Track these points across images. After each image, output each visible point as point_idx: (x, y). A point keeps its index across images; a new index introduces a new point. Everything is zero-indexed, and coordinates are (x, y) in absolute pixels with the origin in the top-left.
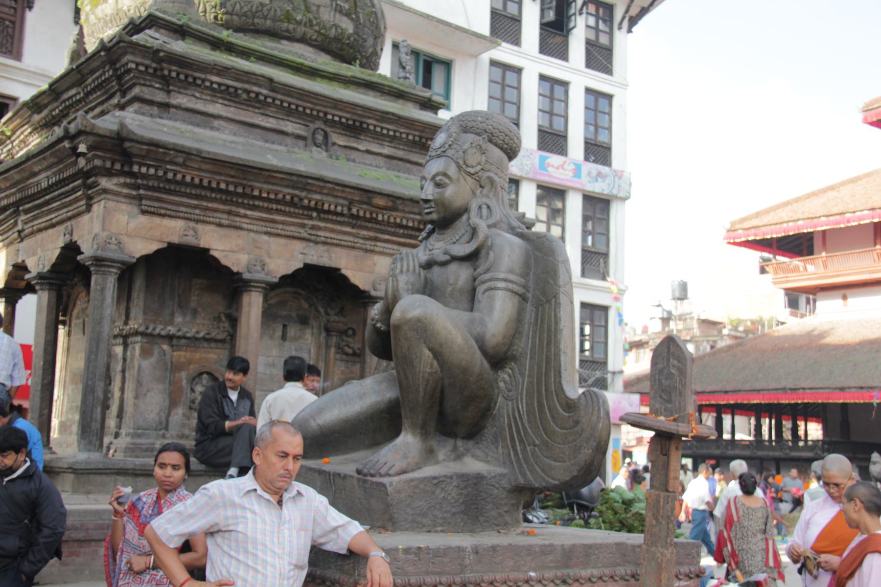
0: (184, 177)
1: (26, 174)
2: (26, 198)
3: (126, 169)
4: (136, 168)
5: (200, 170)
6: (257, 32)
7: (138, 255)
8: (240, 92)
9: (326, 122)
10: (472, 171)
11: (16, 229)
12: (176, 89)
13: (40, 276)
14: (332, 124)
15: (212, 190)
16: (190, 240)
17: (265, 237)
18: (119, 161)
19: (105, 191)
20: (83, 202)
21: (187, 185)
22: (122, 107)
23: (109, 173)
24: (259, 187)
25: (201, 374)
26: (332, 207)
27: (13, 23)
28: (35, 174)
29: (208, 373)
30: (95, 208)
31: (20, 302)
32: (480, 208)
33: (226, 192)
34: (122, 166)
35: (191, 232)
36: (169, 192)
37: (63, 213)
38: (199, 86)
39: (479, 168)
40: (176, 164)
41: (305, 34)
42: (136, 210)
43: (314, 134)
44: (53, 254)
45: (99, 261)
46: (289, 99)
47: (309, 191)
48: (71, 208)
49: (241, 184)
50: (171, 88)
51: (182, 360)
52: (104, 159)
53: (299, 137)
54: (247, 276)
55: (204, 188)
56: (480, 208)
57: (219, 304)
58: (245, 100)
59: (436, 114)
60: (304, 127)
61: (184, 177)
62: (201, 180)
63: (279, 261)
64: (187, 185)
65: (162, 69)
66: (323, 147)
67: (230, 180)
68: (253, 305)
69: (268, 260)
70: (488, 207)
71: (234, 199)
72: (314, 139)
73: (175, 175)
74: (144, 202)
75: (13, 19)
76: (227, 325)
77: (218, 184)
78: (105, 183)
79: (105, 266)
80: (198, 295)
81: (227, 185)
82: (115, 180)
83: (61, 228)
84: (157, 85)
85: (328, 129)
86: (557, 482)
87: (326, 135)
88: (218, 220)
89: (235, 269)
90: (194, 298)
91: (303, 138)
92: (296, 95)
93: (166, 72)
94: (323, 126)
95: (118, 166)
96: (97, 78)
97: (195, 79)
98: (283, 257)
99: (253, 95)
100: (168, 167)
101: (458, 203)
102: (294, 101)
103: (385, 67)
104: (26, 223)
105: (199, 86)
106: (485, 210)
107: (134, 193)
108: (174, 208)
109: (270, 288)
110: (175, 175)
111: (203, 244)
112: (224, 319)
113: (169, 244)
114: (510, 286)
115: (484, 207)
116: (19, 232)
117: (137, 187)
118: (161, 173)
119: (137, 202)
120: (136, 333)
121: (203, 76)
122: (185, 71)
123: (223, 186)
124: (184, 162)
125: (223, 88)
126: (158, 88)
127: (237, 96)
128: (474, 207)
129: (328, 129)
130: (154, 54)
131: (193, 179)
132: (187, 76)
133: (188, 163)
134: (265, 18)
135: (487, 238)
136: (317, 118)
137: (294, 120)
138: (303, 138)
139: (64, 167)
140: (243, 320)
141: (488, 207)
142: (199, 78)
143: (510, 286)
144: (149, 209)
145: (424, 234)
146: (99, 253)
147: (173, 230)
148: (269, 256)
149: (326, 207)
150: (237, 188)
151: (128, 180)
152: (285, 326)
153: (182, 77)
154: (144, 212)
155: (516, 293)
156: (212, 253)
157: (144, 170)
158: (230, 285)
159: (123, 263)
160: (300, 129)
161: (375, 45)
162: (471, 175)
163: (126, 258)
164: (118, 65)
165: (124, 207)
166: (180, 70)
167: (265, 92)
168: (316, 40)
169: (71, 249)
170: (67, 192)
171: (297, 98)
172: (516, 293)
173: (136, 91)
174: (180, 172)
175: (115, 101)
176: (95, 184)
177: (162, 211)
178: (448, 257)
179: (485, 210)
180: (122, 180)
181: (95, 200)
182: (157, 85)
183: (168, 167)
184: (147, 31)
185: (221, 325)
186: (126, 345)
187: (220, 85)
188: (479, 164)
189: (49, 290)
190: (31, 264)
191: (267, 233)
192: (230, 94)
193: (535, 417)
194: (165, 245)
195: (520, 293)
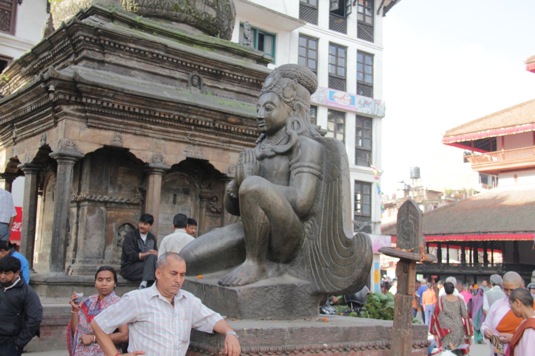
0: (113, 105)
1: (18, 104)
2: (18, 118)
3: (78, 100)
4: (84, 100)
5: (123, 101)
6: (158, 17)
7: (85, 153)
8: (147, 53)
9: (200, 71)
10: (288, 100)
11: (12, 137)
13: (27, 166)
14: (203, 72)
15: (131, 113)
17: (163, 142)
18: (74, 96)
19: (66, 114)
21: (115, 110)
27: (10, 12)
28: (23, 104)
29: (128, 224)
30: (60, 124)
31: (15, 181)
32: (293, 123)
33: (139, 114)
34: (76, 98)
35: (118, 139)
37: (40, 128)
38: (123, 50)
39: (292, 99)
40: (108, 97)
41: (186, 18)
42: (84, 125)
43: (192, 79)
44: (34, 152)
45: (62, 156)
46: (177, 58)
47: (189, 113)
49: (148, 109)
50: (105, 51)
51: (113, 216)
52: (65, 95)
54: (152, 165)
55: (126, 112)
56: (293, 123)
57: (135, 182)
58: (150, 58)
59: (266, 66)
60: (186, 75)
62: (124, 107)
64: (115, 110)
66: (198, 87)
67: (141, 107)
68: (156, 183)
70: (298, 122)
71: (144, 119)
72: (192, 82)
73: (108, 104)
75: (10, 10)
76: (140, 194)
77: (134, 109)
78: (65, 109)
79: (65, 159)
81: (140, 110)
82: (72, 107)
83: (39, 137)
84: (97, 50)
85: (201, 76)
86: (340, 289)
88: (134, 131)
89: (145, 161)
91: (186, 81)
92: (181, 55)
93: (102, 42)
94: (198, 74)
95: (73, 99)
96: (61, 46)
97: (120, 45)
99: (155, 55)
100: (104, 99)
101: (280, 120)
102: (180, 59)
103: (236, 38)
104: (18, 134)
105: (123, 50)
106: (296, 125)
107: (83, 115)
108: (108, 124)
109: (166, 172)
110: (108, 104)
112: (138, 191)
114: (311, 170)
115: (296, 123)
116: (14, 139)
117: (85, 111)
118: (99, 103)
121: (125, 44)
122: (114, 41)
123: (137, 110)
124: (113, 96)
125: (137, 51)
128: (289, 122)
131: (119, 106)
132: (115, 44)
133: (116, 97)
136: (194, 69)
137: (180, 70)
138: (186, 81)
139: (41, 99)
141: (298, 122)
142: (123, 45)
143: (311, 170)
144: (92, 125)
145: (259, 139)
146: (62, 151)
147: (107, 137)
148: (165, 153)
149: (200, 123)
150: (146, 112)
152: (175, 195)
153: (112, 44)
154: (89, 127)
155: (315, 175)
156: (131, 151)
157: (89, 101)
159: (77, 157)
160: (184, 76)
161: (229, 25)
162: (287, 103)
163: (78, 154)
164: (73, 38)
165: (77, 123)
166: (111, 40)
168: (193, 22)
169: (45, 149)
170: (43, 114)
171: (182, 57)
172: (315, 175)
173: (84, 53)
174: (111, 102)
175: (71, 59)
176: (60, 110)
178: (273, 153)
179: (296, 125)
180: (76, 107)
183: (104, 99)
184: (91, 17)
185: (137, 195)
186: (79, 207)
188: (292, 96)
189: (32, 174)
190: (21, 158)
191: (164, 139)
194: (102, 146)
195: (317, 174)
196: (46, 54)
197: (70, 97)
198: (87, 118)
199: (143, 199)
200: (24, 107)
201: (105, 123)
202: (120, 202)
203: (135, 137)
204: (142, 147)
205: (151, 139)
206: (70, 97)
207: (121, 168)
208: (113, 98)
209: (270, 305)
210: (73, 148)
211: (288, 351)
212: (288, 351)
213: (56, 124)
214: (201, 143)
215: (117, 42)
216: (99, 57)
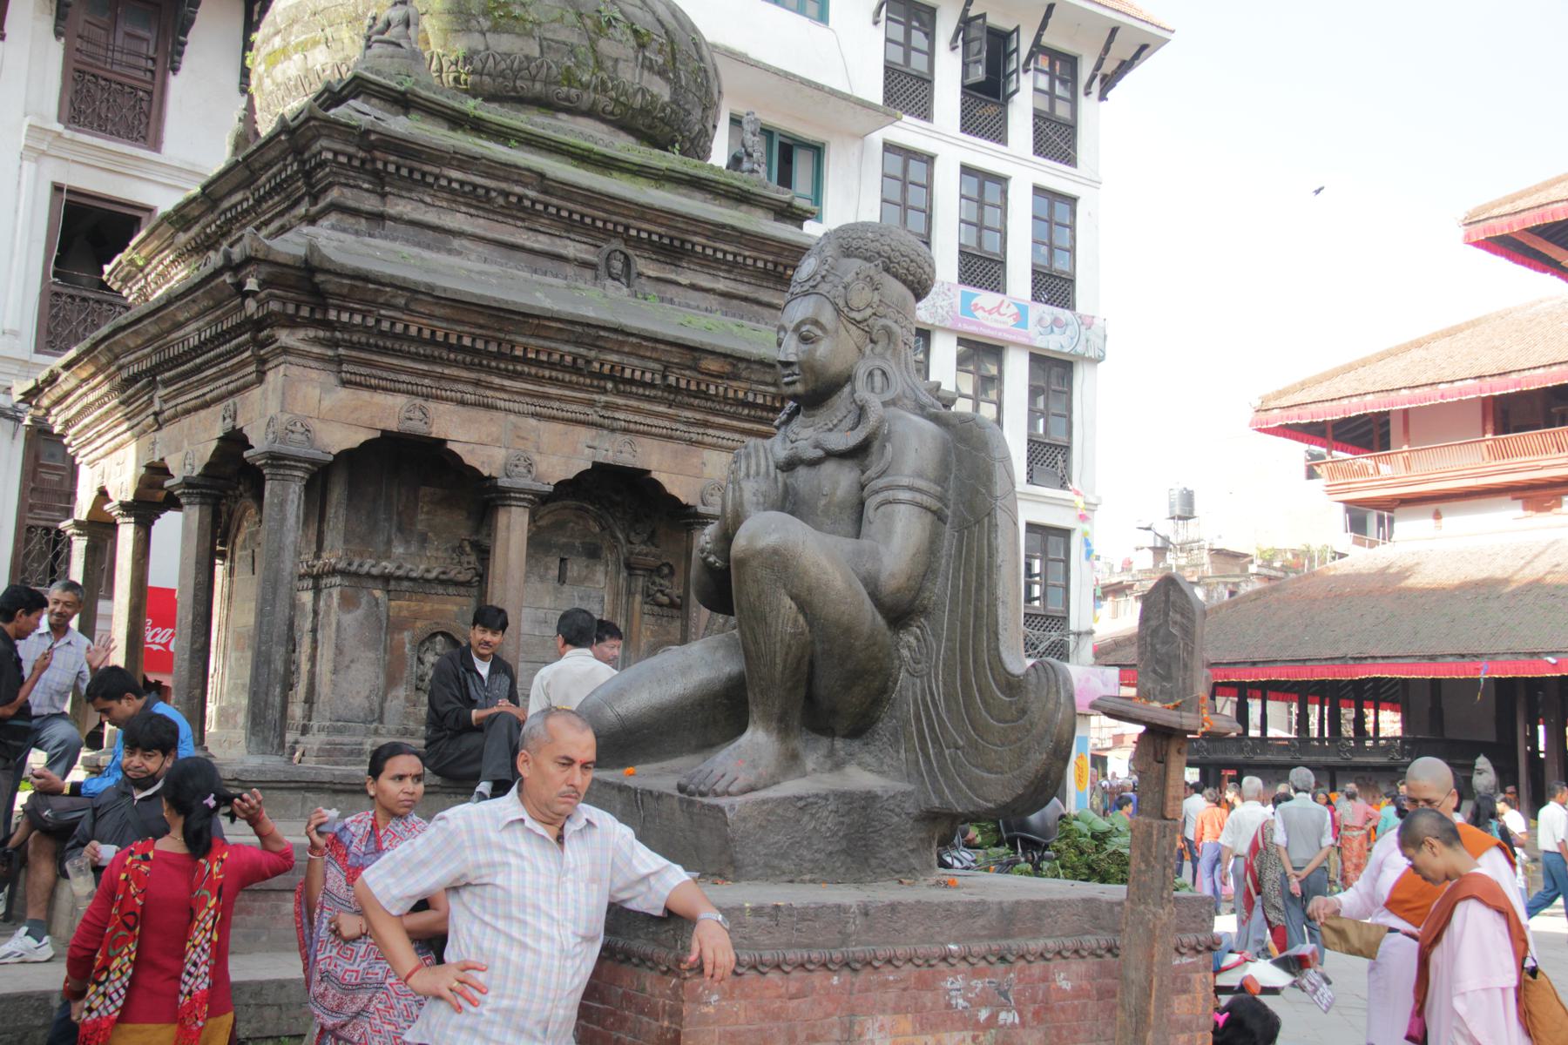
0: (406, 327)
1: (166, 325)
3: (318, 316)
5: (431, 316)
7: (335, 451)
8: (493, 194)
9: (627, 240)
10: (858, 316)
11: (151, 411)
12: (395, 191)
13: (188, 483)
14: (637, 243)
15: (451, 348)
16: (417, 427)
17: (533, 422)
18: (307, 303)
19: (286, 350)
20: (252, 368)
22: (312, 220)
23: (292, 323)
24: (524, 343)
25: (434, 635)
26: (638, 374)
27: (150, 93)
29: (443, 634)
30: (270, 376)
32: (871, 374)
33: (472, 351)
34: (312, 311)
35: (418, 414)
36: (384, 351)
37: (222, 386)
38: (431, 186)
39: (869, 311)
41: (594, 103)
42: (332, 379)
43: (608, 259)
44: (206, 449)
46: (571, 206)
47: (601, 349)
48: (234, 377)
49: (494, 339)
50: (387, 189)
51: (404, 613)
53: (585, 264)
54: (503, 482)
56: (871, 374)
57: (459, 525)
59: (801, 227)
61: (406, 327)
63: (554, 460)
65: (374, 160)
68: (514, 527)
69: (536, 458)
70: (884, 373)
72: (608, 267)
73: (393, 324)
75: (150, 87)
76: (473, 558)
77: (460, 338)
78: (285, 337)
80: (428, 513)
81: (474, 340)
82: (301, 333)
83: (218, 409)
85: (630, 252)
86: (991, 805)
87: (627, 261)
90: (422, 517)
93: (380, 165)
95: (305, 312)
97: (424, 174)
100: (383, 312)
101: (837, 367)
103: (719, 155)
104: (165, 401)
105: (431, 186)
106: (878, 378)
110: (393, 324)
111: (436, 432)
112: (468, 549)
113: (383, 431)
114: (918, 497)
115: (878, 373)
116: (156, 414)
117: (335, 344)
118: (371, 322)
119: (333, 367)
120: (334, 572)
121: (436, 170)
122: (408, 162)
123: (467, 341)
125: (467, 188)
126: (367, 190)
127: (489, 200)
130: (362, 137)
131: (420, 330)
132: (411, 171)
133: (413, 306)
135: (882, 421)
136: (615, 234)
140: (499, 551)
141: (884, 373)
142: (431, 174)
143: (918, 497)
144: (353, 378)
145: (782, 416)
146: (277, 447)
147: (389, 411)
149: (628, 374)
151: (321, 334)
152: (562, 560)
153: (404, 172)
154: (345, 383)
155: (927, 509)
156: (450, 446)
157: (345, 317)
158: (478, 496)
159: (313, 462)
160: (587, 252)
161: (704, 119)
162: (856, 323)
163: (318, 455)
164: (306, 156)
165: (314, 374)
166: (401, 161)
167: (532, 194)
169: (234, 441)
171: (582, 204)
173: (334, 194)
175: (301, 210)
176: (272, 340)
177: (374, 382)
178: (820, 453)
179: (878, 378)
180: (311, 333)
183: (383, 312)
184: (352, 102)
185: (465, 559)
186: (317, 590)
187: (462, 183)
188: (869, 305)
189: (201, 504)
190: (173, 464)
191: (534, 415)
192: (524, 209)
193: (958, 703)
194: (378, 434)
196: (238, 197)
197: (298, 308)
198: (339, 361)
199: (480, 569)
200: (182, 332)
201: (385, 374)
202: (422, 578)
203: (460, 408)
204: (479, 436)
205: (502, 414)
206: (298, 308)
208: (406, 309)
209: (810, 844)
211: (857, 961)
212: (857, 961)
213: (261, 377)
215: (416, 165)
216: (370, 203)
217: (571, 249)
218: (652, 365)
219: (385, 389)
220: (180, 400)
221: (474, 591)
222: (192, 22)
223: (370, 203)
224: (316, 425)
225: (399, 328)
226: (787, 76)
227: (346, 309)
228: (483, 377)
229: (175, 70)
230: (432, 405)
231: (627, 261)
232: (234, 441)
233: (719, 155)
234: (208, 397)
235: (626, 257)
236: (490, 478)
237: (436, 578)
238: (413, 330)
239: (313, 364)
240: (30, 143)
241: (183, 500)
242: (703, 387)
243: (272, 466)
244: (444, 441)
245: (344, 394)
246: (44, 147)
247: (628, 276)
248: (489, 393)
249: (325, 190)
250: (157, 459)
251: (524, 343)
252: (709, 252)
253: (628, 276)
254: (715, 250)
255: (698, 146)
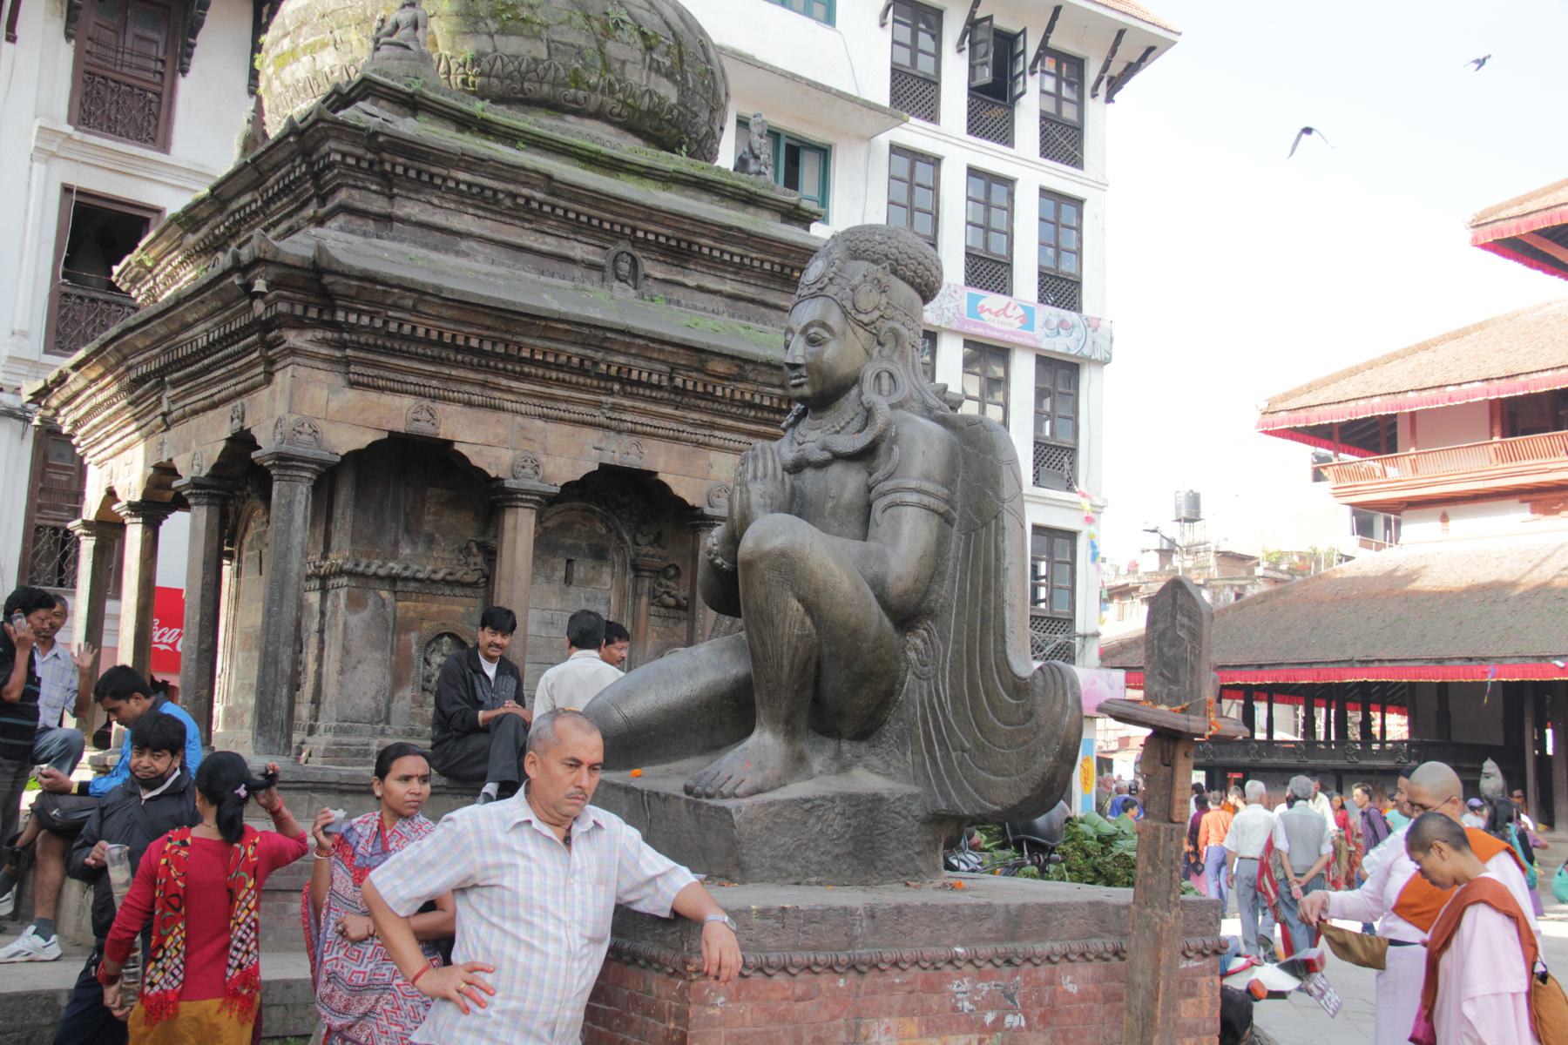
0: (414, 328)
2: (174, 362)
4: (340, 316)
5: (439, 318)
7: (342, 452)
8: (501, 196)
9: (634, 242)
10: (865, 319)
11: (159, 411)
12: (403, 193)
13: (196, 484)
14: (644, 245)
15: (458, 349)
16: (424, 428)
17: (540, 423)
18: (315, 305)
19: (294, 351)
20: (261, 369)
23: (300, 324)
24: (532, 344)
25: (441, 636)
27: (159, 95)
28: (189, 326)
29: (450, 635)
30: (278, 377)
32: (878, 376)
33: (479, 352)
34: (320, 312)
35: (425, 415)
36: (392, 352)
37: (230, 386)
38: (439, 187)
39: (876, 314)
40: (402, 309)
43: (615, 261)
44: (213, 449)
46: (578, 207)
47: (608, 350)
49: (502, 340)
51: (411, 614)
53: (592, 266)
54: (510, 483)
56: (878, 376)
57: (466, 526)
59: (808, 229)
61: (414, 328)
62: (441, 334)
63: (561, 461)
65: (382, 162)
67: (486, 333)
68: (521, 528)
69: (543, 459)
70: (891, 376)
72: (615, 268)
73: (400, 326)
74: (352, 368)
75: (159, 89)
76: (479, 559)
78: (293, 338)
82: (309, 335)
83: (226, 409)
85: (637, 254)
87: (634, 263)
92: (587, 201)
93: (388, 167)
95: (313, 313)
97: (432, 176)
98: (565, 452)
101: (845, 369)
102: (586, 210)
103: (726, 157)
104: (174, 402)
105: (439, 187)
109: (547, 503)
110: (400, 326)
111: (443, 433)
112: (475, 550)
113: (391, 432)
114: (926, 500)
115: (885, 376)
116: (164, 415)
117: (343, 345)
118: (378, 323)
119: (342, 369)
120: (341, 572)
122: (416, 164)
123: (474, 343)
125: (475, 190)
127: (497, 202)
129: (637, 254)
130: (369, 138)
132: (419, 173)
133: (421, 308)
134: (541, 81)
135: (889, 424)
136: (622, 236)
140: (505, 552)
141: (891, 376)
142: (439, 176)
143: (926, 500)
144: (361, 379)
146: (284, 448)
147: (396, 412)
149: (634, 375)
152: (569, 561)
153: (412, 174)
154: (353, 384)
156: (457, 447)
157: (353, 318)
158: (485, 497)
159: (321, 463)
160: (594, 254)
162: (864, 325)
163: (326, 456)
164: (314, 157)
165: (322, 375)
166: (409, 163)
167: (539, 195)
169: (242, 442)
173: (342, 196)
176: (278, 341)
180: (319, 334)
181: (278, 366)
182: (374, 187)
184: (360, 104)
185: (471, 560)
186: (324, 591)
187: (470, 185)
188: (877, 308)
189: (209, 504)
190: (181, 464)
191: (541, 417)
192: (531, 211)
194: (385, 435)
196: (246, 198)
197: (306, 309)
198: (347, 362)
199: (486, 569)
200: (190, 333)
203: (467, 410)
204: (486, 437)
206: (306, 309)
207: (432, 492)
208: (414, 310)
210: (310, 439)
213: (269, 378)
214: (639, 428)
215: (424, 166)
216: (378, 205)
217: (578, 250)
218: (658, 366)
219: (392, 390)
220: (188, 401)
221: (481, 592)
222: (201, 24)
223: (378, 205)
224: (323, 426)
225: (407, 329)
226: (793, 77)
227: (354, 310)
228: (491, 378)
229: (184, 72)
230: (439, 407)
231: (634, 263)
232: (242, 442)
233: (726, 157)
234: (216, 398)
235: (633, 259)
236: (497, 479)
237: (443, 580)
238: (421, 332)
239: (320, 365)
240: (41, 145)
241: (191, 501)
242: (710, 389)
243: (280, 467)
244: (451, 442)
245: (352, 395)
246: (54, 149)
247: (635, 278)
248: (497, 394)
249: (334, 191)
250: (165, 460)
251: (532, 344)
252: (716, 253)
253: (635, 278)
254: (722, 252)
255: (705, 148)
